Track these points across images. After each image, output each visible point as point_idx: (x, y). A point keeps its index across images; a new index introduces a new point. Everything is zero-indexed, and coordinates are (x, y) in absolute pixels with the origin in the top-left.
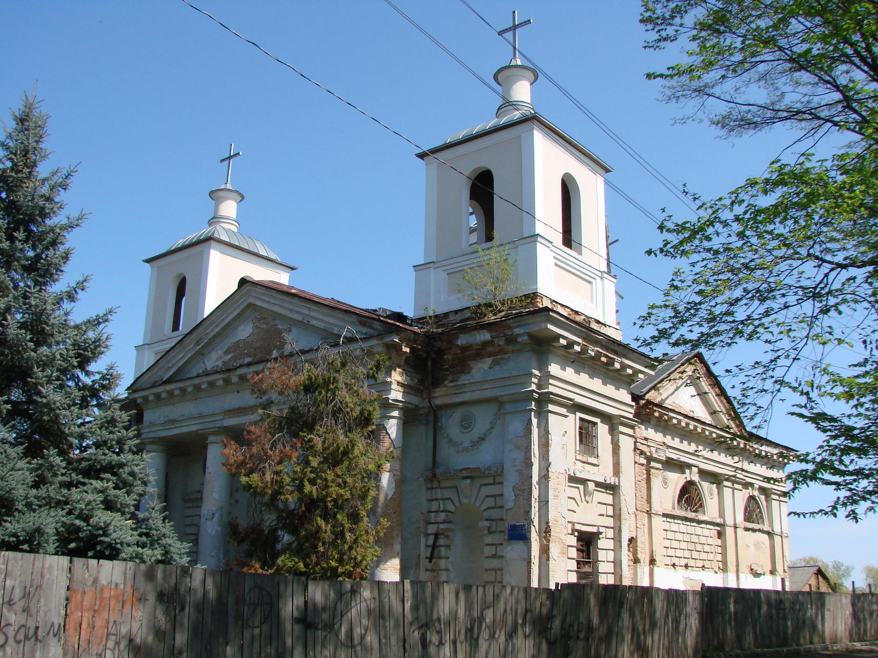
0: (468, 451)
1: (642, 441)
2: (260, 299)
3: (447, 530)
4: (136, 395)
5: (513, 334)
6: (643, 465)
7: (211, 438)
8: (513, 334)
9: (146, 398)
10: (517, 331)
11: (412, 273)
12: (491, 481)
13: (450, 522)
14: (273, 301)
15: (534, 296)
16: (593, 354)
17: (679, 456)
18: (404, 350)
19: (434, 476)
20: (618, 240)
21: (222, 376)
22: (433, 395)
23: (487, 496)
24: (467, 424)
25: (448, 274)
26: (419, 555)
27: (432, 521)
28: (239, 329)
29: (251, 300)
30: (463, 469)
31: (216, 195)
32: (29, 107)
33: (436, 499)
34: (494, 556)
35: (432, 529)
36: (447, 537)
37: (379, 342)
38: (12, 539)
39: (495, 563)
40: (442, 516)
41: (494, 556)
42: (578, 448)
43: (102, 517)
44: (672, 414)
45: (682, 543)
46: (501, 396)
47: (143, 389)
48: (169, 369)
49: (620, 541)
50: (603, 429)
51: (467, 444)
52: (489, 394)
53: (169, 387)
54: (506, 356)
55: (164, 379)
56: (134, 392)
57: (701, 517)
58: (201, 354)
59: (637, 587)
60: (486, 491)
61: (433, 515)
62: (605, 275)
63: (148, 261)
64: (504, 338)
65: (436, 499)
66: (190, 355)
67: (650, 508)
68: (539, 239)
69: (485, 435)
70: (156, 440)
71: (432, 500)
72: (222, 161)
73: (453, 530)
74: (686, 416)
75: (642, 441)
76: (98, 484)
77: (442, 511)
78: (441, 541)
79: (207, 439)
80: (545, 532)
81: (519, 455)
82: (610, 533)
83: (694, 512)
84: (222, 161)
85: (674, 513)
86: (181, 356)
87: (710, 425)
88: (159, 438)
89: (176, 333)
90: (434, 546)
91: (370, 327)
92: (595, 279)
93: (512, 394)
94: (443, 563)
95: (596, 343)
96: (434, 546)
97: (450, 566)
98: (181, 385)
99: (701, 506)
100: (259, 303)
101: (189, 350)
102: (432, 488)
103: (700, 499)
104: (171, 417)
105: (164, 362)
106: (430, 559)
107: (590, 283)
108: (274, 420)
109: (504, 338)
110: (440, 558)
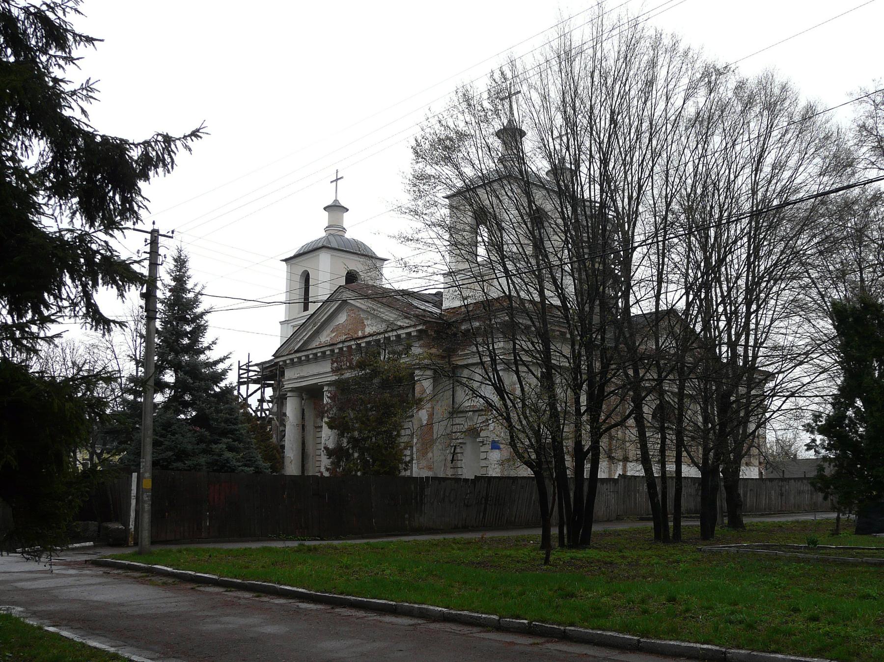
4: (278, 360)
9: (285, 361)
21: (329, 348)
32: (180, 251)
38: (676, 256)
43: (228, 455)
47: (282, 356)
53: (298, 355)
58: (317, 333)
59: (457, 480)
63: (286, 260)
72: (332, 182)
73: (465, 443)
76: (225, 440)
78: (458, 450)
84: (332, 182)
89: (306, 313)
90: (454, 454)
94: (459, 464)
96: (454, 454)
97: (463, 466)
98: (305, 353)
106: (452, 461)
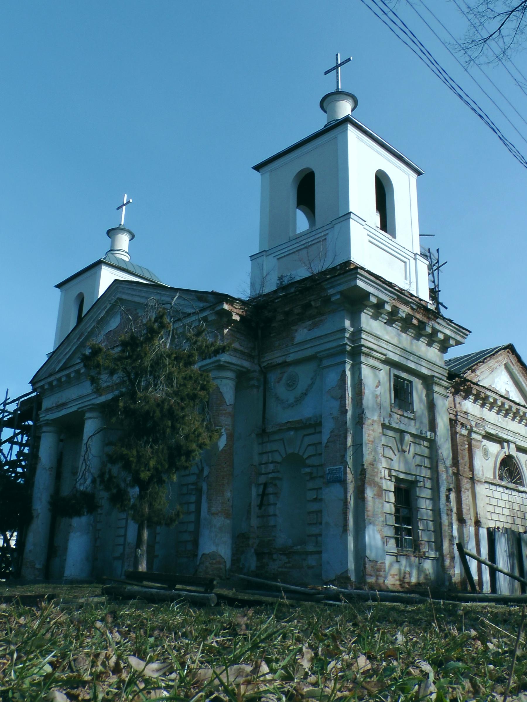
0: (293, 406)
1: (462, 415)
2: (127, 294)
3: (274, 478)
5: (327, 295)
6: (464, 436)
7: (87, 415)
8: (327, 295)
10: (331, 291)
11: (248, 263)
12: (312, 431)
13: (278, 472)
14: (134, 293)
15: (348, 263)
16: (404, 316)
17: (497, 432)
18: (233, 318)
19: (264, 431)
20: (434, 236)
22: (262, 360)
23: (309, 445)
24: (292, 384)
25: (278, 259)
26: (250, 503)
27: (263, 472)
28: (111, 322)
29: (119, 295)
30: (288, 422)
31: (112, 233)
33: (266, 453)
34: (315, 500)
35: (262, 479)
36: (275, 485)
37: (211, 312)
39: (315, 507)
40: (271, 467)
41: (315, 500)
42: (393, 402)
44: (489, 393)
45: (500, 501)
46: (320, 352)
48: (59, 362)
49: (439, 491)
50: (418, 385)
51: (292, 400)
52: (309, 352)
54: (323, 318)
55: (57, 370)
56: (37, 382)
57: (521, 488)
60: (307, 440)
61: (263, 466)
62: (418, 257)
64: (320, 300)
65: (266, 453)
66: (74, 348)
67: (473, 474)
68: (352, 216)
69: (307, 390)
70: (49, 422)
71: (263, 453)
74: (501, 396)
75: (462, 415)
77: (272, 462)
78: (270, 490)
79: (84, 415)
80: (361, 475)
81: (336, 404)
82: (428, 484)
83: (514, 483)
85: (495, 482)
86: (68, 350)
87: (524, 406)
88: (52, 420)
91: (206, 301)
92: (409, 260)
93: (329, 349)
95: (406, 303)
99: (521, 478)
100: (124, 297)
101: (74, 344)
102: (263, 443)
103: (518, 474)
104: (61, 402)
105: (56, 356)
107: (405, 262)
108: (469, 634)
109: (320, 300)
110: (269, 505)
